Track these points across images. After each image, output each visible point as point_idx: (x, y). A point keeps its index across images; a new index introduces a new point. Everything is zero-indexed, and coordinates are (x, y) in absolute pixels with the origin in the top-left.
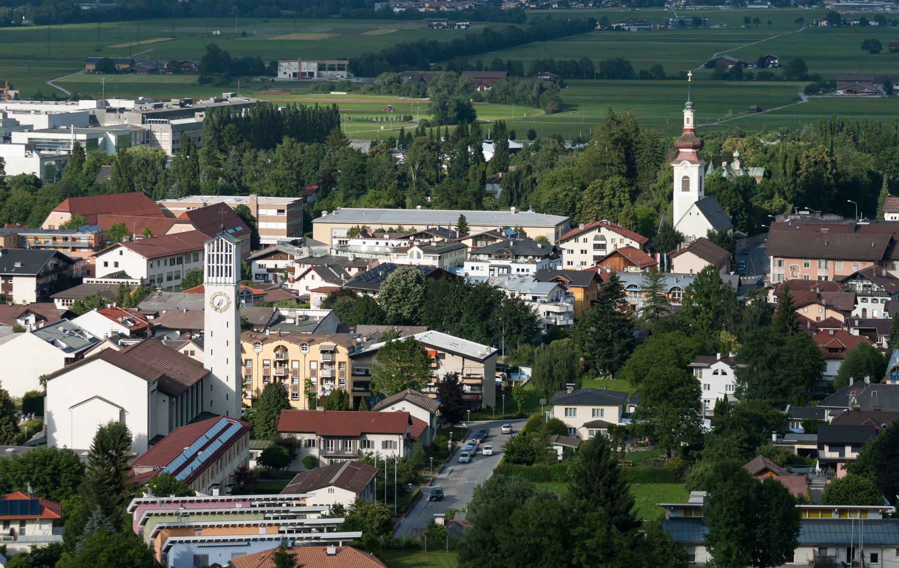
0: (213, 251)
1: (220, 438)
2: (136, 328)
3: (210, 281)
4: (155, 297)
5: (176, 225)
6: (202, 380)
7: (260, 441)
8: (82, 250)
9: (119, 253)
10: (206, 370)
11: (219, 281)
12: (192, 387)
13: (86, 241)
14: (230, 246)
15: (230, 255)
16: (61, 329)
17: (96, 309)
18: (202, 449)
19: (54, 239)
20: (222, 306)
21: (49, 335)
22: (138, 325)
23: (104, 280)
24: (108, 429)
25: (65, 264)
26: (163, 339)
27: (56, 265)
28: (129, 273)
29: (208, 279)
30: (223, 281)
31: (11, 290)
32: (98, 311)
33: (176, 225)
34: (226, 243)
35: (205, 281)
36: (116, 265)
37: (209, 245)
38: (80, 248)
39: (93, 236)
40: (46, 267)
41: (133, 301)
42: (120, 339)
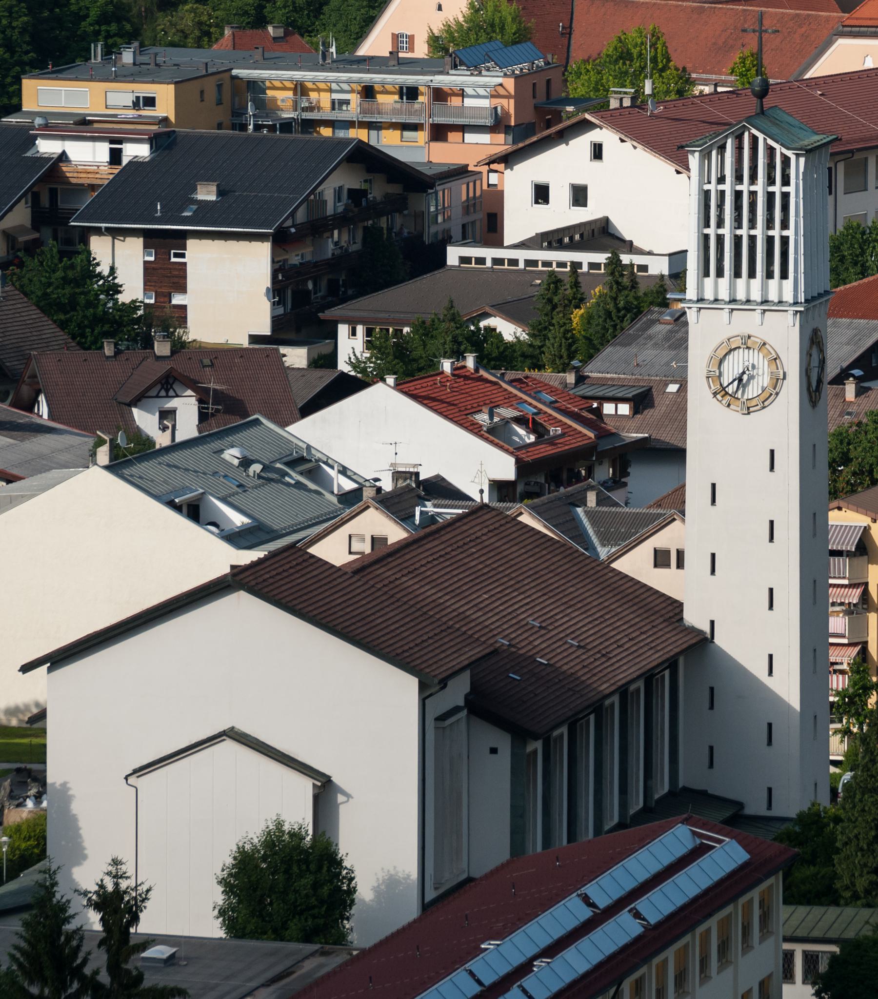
0: (721, 180)
1: (641, 905)
2: (546, 450)
3: (709, 295)
4: (659, 329)
5: (842, 43)
6: (672, 664)
7: (849, 911)
8: (470, 138)
9: (587, 151)
10: (693, 630)
11: (741, 295)
12: (623, 692)
13: (485, 103)
14: (786, 161)
15: (785, 196)
16: (232, 455)
17: (390, 380)
18: (552, 950)
19: (368, 92)
20: (753, 390)
21: (178, 479)
22: (552, 441)
23: (522, 255)
24: (264, 858)
25: (395, 189)
26: (583, 502)
27: (355, 195)
28: (625, 228)
29: (700, 287)
30: (756, 296)
31: (182, 288)
32: (398, 386)
33: (841, 42)
34: (771, 151)
35: (691, 293)
36: (579, 196)
37: (706, 155)
38: (463, 129)
39: (510, 84)
40: (316, 203)
41: (581, 344)
42: (421, 500)
